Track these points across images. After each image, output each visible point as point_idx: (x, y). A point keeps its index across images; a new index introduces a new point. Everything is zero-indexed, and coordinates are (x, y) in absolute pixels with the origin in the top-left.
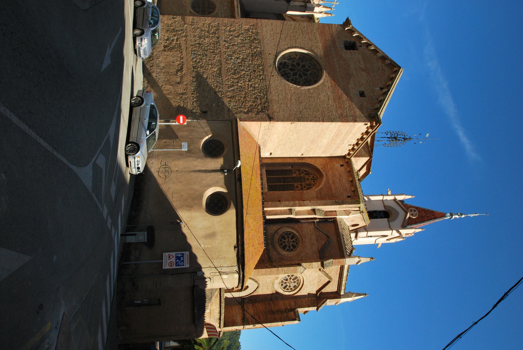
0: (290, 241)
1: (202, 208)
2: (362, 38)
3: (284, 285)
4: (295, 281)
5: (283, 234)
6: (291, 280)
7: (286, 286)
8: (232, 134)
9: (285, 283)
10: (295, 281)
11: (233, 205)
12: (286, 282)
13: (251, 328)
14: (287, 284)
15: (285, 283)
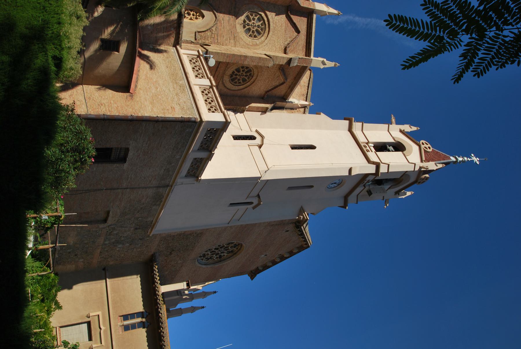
0: (241, 74)
1: (166, 19)
2: (179, 44)
3: (256, 33)
4: (252, 19)
5: (242, 84)
6: (250, 23)
7: (257, 30)
8: (299, 149)
9: (253, 32)
10: (252, 19)
11: (251, 104)
12: (252, 30)
13: (100, 346)
14: (254, 29)
15: (253, 32)
